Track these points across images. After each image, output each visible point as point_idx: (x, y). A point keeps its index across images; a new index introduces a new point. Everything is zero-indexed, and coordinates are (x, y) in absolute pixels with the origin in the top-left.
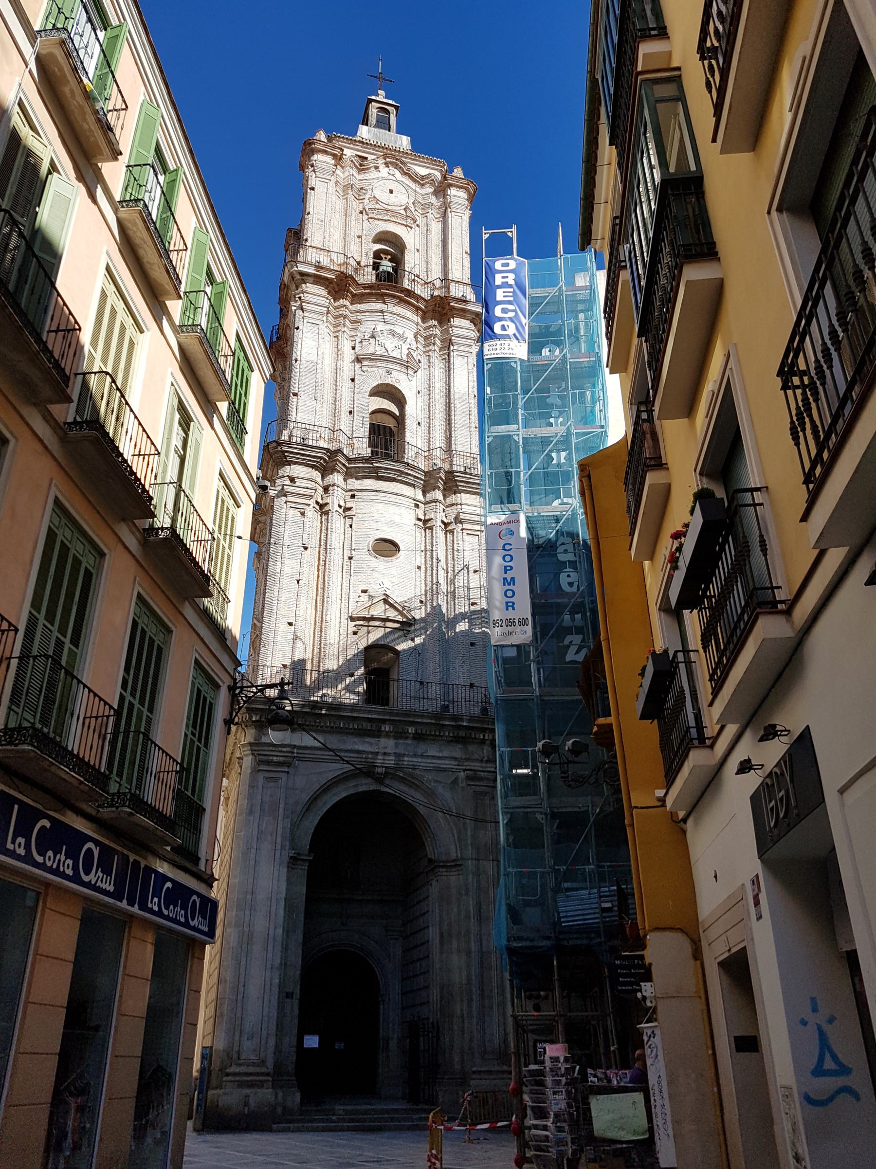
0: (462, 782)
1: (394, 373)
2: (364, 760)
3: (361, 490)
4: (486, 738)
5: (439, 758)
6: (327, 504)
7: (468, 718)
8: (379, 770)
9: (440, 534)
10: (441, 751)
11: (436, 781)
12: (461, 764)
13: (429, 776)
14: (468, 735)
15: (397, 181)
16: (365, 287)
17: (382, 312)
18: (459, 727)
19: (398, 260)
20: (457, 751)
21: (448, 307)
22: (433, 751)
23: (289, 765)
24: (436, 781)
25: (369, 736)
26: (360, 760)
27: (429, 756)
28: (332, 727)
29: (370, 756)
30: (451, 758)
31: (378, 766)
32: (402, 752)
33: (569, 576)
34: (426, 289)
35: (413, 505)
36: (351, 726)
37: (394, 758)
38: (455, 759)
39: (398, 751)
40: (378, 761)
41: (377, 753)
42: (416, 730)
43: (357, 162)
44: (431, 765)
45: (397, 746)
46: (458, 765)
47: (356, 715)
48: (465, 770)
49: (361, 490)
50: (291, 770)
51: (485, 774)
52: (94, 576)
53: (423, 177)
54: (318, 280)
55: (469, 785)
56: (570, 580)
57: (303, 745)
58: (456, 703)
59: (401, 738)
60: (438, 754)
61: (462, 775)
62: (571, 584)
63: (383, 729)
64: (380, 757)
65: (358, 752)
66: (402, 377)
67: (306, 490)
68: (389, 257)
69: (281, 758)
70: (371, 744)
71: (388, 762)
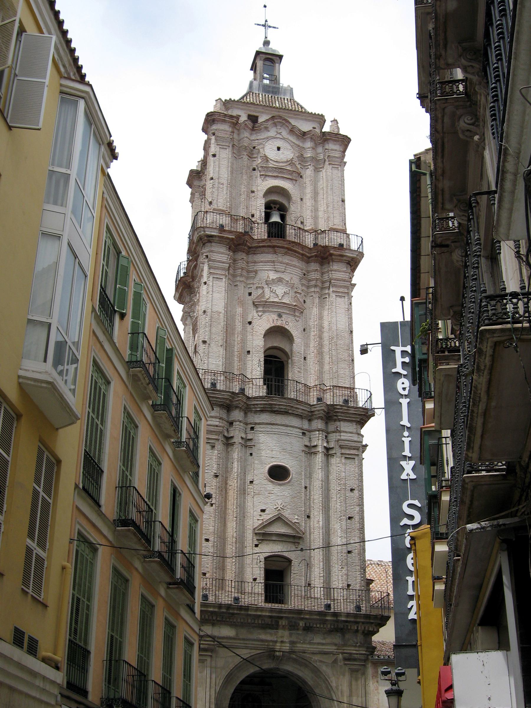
0: (340, 662)
1: (284, 316)
2: (266, 647)
3: (259, 424)
4: (359, 628)
5: (323, 644)
6: (232, 437)
7: (345, 614)
8: (278, 654)
9: (319, 458)
10: (324, 639)
11: (321, 661)
12: (340, 648)
13: (316, 658)
14: (345, 627)
15: (284, 139)
16: (259, 242)
17: (273, 262)
18: (338, 621)
19: (283, 210)
20: (337, 639)
21: (328, 253)
22: (318, 639)
23: (212, 651)
24: (321, 661)
25: (270, 628)
26: (263, 646)
27: (315, 643)
28: (242, 623)
29: (271, 644)
30: (331, 644)
31: (277, 651)
32: (295, 640)
33: (403, 383)
34: (309, 236)
35: (301, 434)
36: (256, 622)
37: (288, 645)
38: (336, 645)
39: (292, 639)
40: (277, 647)
41: (276, 642)
42: (306, 624)
43: (250, 124)
44: (317, 650)
45: (291, 635)
46: (337, 649)
47: (260, 613)
48: (342, 653)
49: (259, 424)
50: (214, 655)
51: (358, 655)
52: (51, 505)
53: (304, 134)
54: (221, 240)
55: (345, 664)
56: (404, 386)
57: (220, 635)
58: (336, 601)
59: (294, 629)
60: (322, 641)
61: (340, 656)
62: (404, 389)
63: (280, 623)
64: (278, 644)
65: (262, 641)
66: (290, 319)
67: (216, 428)
68: (278, 206)
69: (206, 646)
70: (271, 634)
71: (284, 648)
